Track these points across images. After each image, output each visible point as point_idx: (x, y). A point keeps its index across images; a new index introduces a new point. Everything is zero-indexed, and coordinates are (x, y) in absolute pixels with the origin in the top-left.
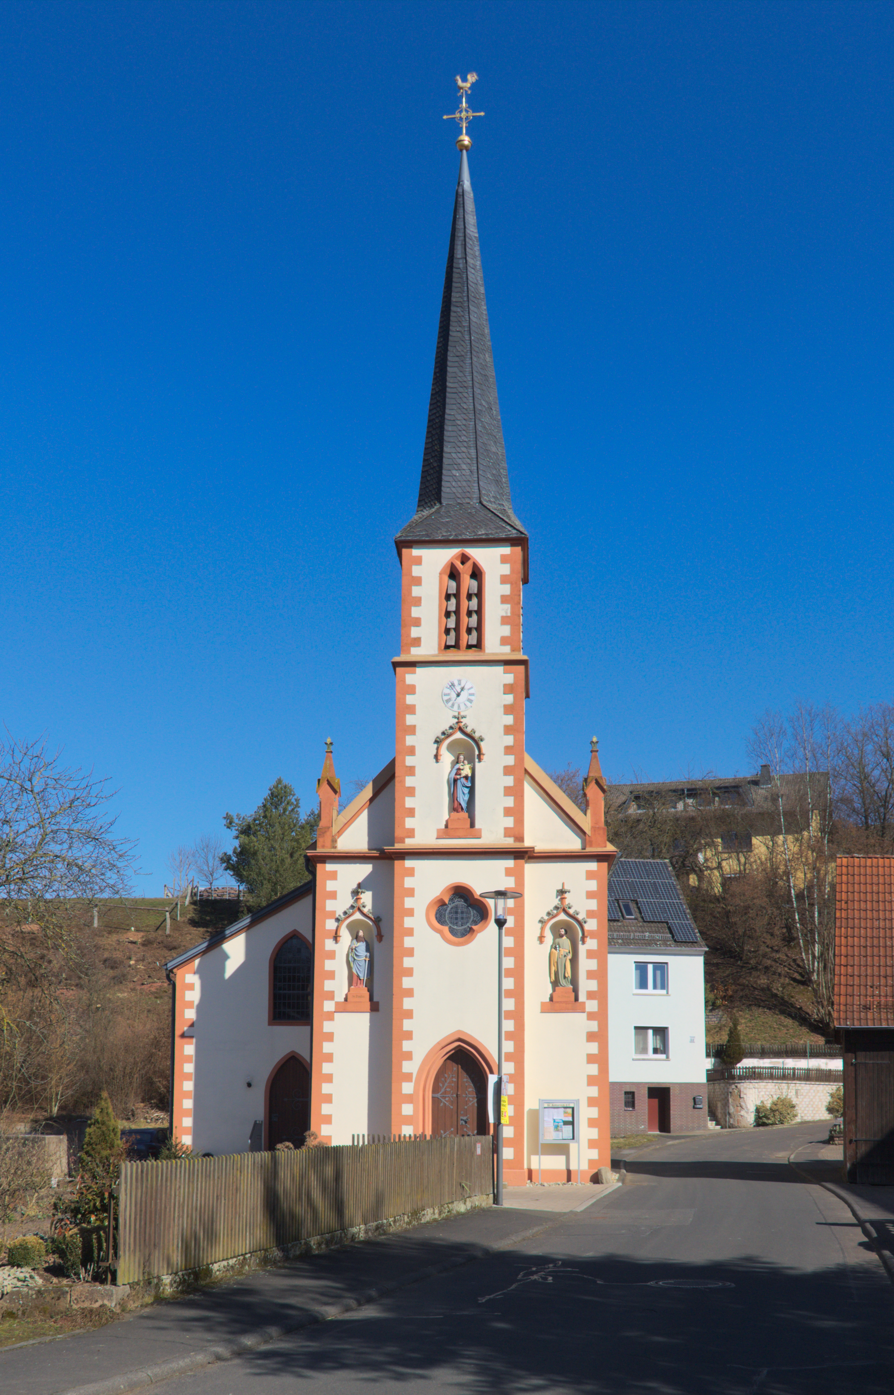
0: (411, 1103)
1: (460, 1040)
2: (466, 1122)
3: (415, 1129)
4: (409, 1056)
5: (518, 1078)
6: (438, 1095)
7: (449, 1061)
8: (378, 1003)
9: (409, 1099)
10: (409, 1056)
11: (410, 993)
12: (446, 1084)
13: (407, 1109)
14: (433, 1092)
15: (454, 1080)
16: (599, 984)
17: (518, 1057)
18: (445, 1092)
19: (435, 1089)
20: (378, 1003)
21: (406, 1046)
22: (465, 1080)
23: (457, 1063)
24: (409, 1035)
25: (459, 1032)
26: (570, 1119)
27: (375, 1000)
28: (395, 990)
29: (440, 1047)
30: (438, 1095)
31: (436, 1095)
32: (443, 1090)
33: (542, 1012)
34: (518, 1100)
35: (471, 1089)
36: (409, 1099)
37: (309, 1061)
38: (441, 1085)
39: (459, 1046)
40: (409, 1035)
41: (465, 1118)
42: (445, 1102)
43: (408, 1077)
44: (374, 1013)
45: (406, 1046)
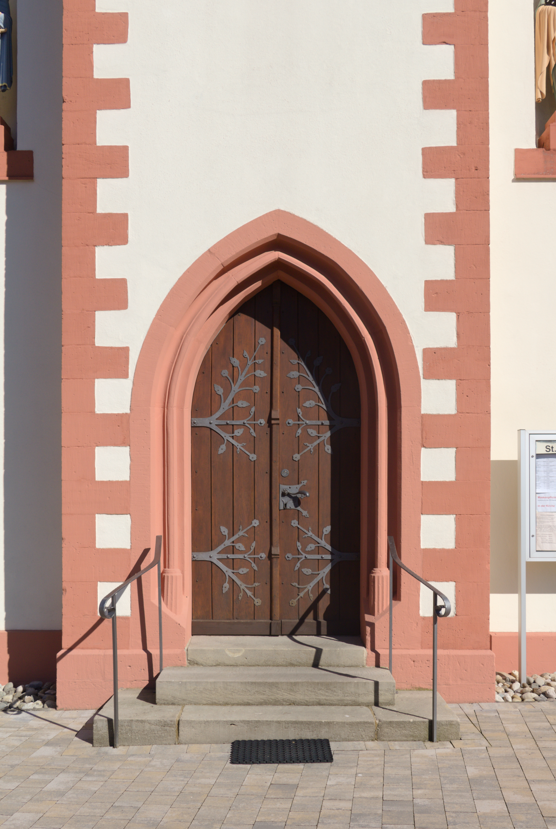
0: (123, 443)
1: (280, 243)
2: (297, 502)
3: (136, 532)
4: (115, 294)
5: (469, 363)
6: (212, 421)
7: (242, 318)
8: (29, 155)
9: (117, 430)
10: (115, 294)
11: (117, 94)
12: (236, 388)
13: (112, 464)
14: (196, 411)
15: (261, 373)
16: (462, 396)
17: (465, 295)
18: (233, 411)
19: (202, 404)
20: (29, 155)
21: (108, 262)
22: (295, 373)
23: (271, 326)
24: (115, 230)
25: (278, 215)
26: (272, 634)
27: (21, 146)
28: (69, 86)
29: (217, 267)
30: (212, 421)
31: (204, 422)
32: (226, 406)
33: (518, 179)
34: (469, 428)
35: (313, 401)
36: (117, 430)
37: (296, 634)
38: (220, 390)
39: (278, 264)
40: (115, 230)
41: (294, 489)
42: (235, 440)
43: (113, 362)
44: (20, 185)
45: (108, 262)
